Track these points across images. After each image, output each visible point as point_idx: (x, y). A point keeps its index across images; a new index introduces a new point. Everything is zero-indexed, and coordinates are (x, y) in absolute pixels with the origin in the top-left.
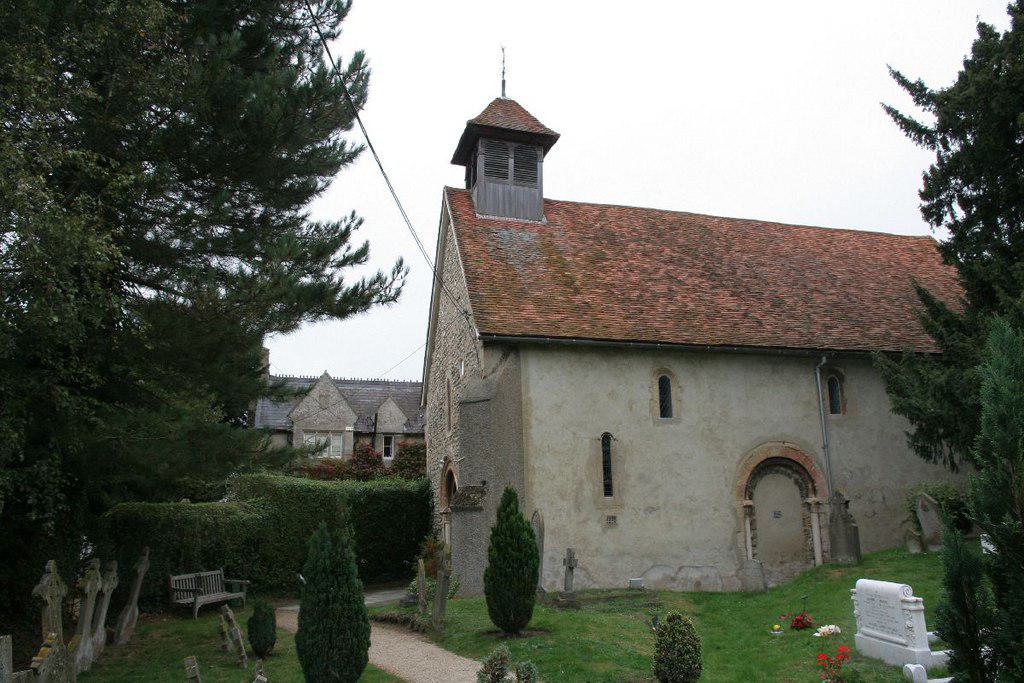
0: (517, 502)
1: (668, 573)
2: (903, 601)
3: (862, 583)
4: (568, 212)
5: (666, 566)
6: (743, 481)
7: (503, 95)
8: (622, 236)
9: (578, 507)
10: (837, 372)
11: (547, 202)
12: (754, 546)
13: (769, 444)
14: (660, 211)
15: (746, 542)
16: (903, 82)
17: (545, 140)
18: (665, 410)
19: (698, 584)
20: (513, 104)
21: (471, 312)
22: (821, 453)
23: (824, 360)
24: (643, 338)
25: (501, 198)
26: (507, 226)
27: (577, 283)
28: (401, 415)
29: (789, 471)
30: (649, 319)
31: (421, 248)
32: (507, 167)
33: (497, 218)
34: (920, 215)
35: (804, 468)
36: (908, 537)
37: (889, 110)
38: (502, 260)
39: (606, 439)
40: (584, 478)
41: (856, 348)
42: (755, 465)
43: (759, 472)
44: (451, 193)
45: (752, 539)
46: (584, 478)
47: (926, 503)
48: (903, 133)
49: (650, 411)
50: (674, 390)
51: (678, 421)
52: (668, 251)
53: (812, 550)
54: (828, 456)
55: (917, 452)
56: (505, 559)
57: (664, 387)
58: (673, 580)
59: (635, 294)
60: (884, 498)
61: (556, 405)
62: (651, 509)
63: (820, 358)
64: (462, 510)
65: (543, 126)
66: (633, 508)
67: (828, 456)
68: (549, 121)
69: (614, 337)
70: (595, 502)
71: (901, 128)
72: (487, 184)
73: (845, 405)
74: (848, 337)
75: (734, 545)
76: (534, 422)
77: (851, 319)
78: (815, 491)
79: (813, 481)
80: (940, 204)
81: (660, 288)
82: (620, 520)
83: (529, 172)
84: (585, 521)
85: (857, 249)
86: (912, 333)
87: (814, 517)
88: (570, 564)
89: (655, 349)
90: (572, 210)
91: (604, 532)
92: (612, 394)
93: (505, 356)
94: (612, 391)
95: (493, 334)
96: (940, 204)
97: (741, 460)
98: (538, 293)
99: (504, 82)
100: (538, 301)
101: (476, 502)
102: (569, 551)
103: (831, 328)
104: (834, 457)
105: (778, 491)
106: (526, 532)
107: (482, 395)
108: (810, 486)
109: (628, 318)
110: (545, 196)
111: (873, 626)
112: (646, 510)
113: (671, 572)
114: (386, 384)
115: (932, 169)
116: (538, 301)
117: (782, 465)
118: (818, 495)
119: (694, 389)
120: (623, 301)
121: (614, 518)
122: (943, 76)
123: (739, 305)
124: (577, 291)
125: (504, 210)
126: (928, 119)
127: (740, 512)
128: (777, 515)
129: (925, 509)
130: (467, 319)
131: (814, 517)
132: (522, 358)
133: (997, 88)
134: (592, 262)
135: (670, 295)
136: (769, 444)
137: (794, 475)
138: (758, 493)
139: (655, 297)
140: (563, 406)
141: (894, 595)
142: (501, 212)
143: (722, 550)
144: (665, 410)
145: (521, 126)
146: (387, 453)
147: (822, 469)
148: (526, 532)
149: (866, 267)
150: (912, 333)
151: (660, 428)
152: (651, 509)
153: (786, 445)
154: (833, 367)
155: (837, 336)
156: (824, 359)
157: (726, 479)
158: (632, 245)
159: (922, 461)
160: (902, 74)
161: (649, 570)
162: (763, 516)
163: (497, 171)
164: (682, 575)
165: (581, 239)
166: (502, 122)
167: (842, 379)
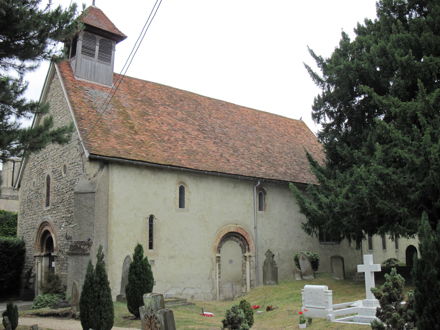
2: (326, 292)
3: (307, 286)
6: (217, 244)
7: (94, 4)
8: (156, 102)
10: (264, 191)
11: (115, 74)
12: (219, 277)
13: (231, 225)
14: (174, 89)
16: (314, 55)
18: (182, 205)
20: (99, 11)
23: (259, 183)
24: (174, 164)
25: (89, 69)
26: (93, 87)
27: (136, 128)
29: (237, 239)
32: (94, 51)
34: (311, 116)
36: (294, 272)
37: (307, 66)
38: (94, 109)
39: (151, 218)
41: (273, 178)
43: (224, 239)
45: (219, 274)
47: (304, 256)
48: (311, 79)
52: (179, 113)
53: (245, 279)
54: (256, 233)
55: (305, 230)
57: (182, 190)
58: (181, 294)
59: (166, 138)
60: (279, 254)
62: (172, 257)
64: (76, 254)
65: (117, 29)
67: (256, 233)
69: (160, 162)
71: (311, 76)
72: (82, 59)
74: (269, 172)
75: (210, 277)
77: (270, 162)
78: (249, 250)
79: (248, 245)
80: (320, 114)
81: (179, 135)
83: (107, 55)
85: (270, 123)
86: (297, 172)
87: (248, 263)
89: (180, 171)
93: (102, 168)
95: (97, 155)
96: (320, 114)
100: (117, 137)
101: (84, 250)
103: (261, 166)
104: (259, 232)
105: (232, 249)
108: (247, 247)
109: (164, 151)
110: (114, 71)
111: (309, 303)
112: (169, 258)
113: (180, 291)
115: (319, 97)
116: (117, 137)
117: (234, 236)
118: (251, 252)
119: (196, 191)
121: (153, 261)
122: (327, 54)
123: (218, 149)
124: (136, 133)
125: (91, 77)
126: (320, 73)
127: (214, 260)
128: (231, 261)
129: (303, 259)
132: (110, 172)
133: (352, 69)
134: (141, 116)
135: (184, 140)
136: (231, 225)
138: (222, 250)
139: (177, 140)
141: (322, 290)
142: (89, 77)
144: (182, 205)
145: (105, 28)
147: (253, 239)
149: (275, 134)
150: (297, 172)
152: (172, 257)
153: (238, 226)
154: (262, 186)
155: (264, 171)
158: (161, 108)
159: (307, 235)
160: (314, 51)
162: (224, 261)
165: (134, 101)
167: (265, 194)
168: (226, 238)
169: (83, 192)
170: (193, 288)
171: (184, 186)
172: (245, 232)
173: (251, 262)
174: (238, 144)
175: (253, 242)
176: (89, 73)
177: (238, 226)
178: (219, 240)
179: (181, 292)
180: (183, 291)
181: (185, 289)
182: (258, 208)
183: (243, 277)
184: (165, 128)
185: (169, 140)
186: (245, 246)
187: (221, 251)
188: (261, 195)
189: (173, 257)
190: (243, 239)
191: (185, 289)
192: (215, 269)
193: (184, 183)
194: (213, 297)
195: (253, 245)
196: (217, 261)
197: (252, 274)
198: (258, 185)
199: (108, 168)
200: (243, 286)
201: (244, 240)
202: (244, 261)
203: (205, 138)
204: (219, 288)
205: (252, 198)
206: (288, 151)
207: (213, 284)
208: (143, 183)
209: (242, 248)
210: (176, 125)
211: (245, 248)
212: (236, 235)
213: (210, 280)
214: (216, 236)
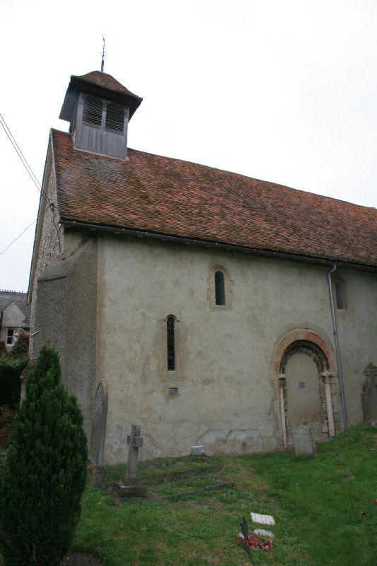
0: (57, 367)
1: (220, 436)
4: (145, 157)
5: (219, 430)
6: (278, 359)
7: (102, 70)
9: (144, 379)
12: (286, 411)
15: (280, 408)
17: (132, 102)
18: (220, 299)
19: (244, 444)
21: (56, 205)
22: (332, 338)
25: (94, 138)
26: (97, 157)
28: (22, 315)
29: (310, 352)
30: (207, 228)
31: (22, 158)
32: (100, 117)
33: (90, 152)
35: (321, 350)
39: (171, 320)
40: (150, 353)
42: (287, 346)
43: (289, 352)
44: (55, 134)
45: (285, 405)
46: (150, 353)
49: (208, 298)
50: (227, 284)
51: (231, 308)
53: (326, 412)
54: (337, 340)
56: (29, 458)
57: (219, 279)
58: (225, 442)
59: (196, 211)
61: (128, 288)
62: (207, 382)
63: (332, 267)
66: (193, 381)
67: (337, 340)
68: (133, 88)
70: (160, 375)
73: (346, 304)
76: (107, 302)
79: (327, 359)
81: (216, 210)
82: (180, 391)
84: (151, 392)
87: (327, 387)
88: (135, 441)
90: (150, 159)
91: (167, 401)
92: (176, 283)
93: (84, 242)
94: (177, 280)
97: (278, 341)
98: (118, 200)
99: (103, 62)
102: (134, 427)
104: (340, 339)
105: (302, 366)
106: (66, 416)
107: (59, 274)
110: (129, 146)
113: (222, 435)
114: (14, 294)
119: (246, 284)
120: (187, 214)
121: (176, 389)
128: (302, 385)
130: (53, 210)
131: (327, 387)
137: (313, 355)
138: (288, 367)
139: (211, 214)
140: (134, 287)
143: (263, 415)
144: (220, 299)
146: (10, 341)
148: (66, 416)
151: (215, 313)
152: (207, 382)
153: (309, 330)
156: (335, 267)
157: (266, 356)
161: (205, 434)
162: (292, 386)
163: (92, 119)
164: (231, 437)
166: (99, 82)
168: (291, 349)
169: (49, 279)
170: (244, 430)
171: (222, 271)
172: (320, 341)
173: (333, 386)
174: (299, 223)
175: (333, 355)
176: (94, 143)
177: (309, 330)
178: (282, 352)
179: (225, 438)
180: (227, 436)
181: (231, 432)
182: (336, 305)
183: (322, 408)
184: (196, 201)
185: (200, 213)
186: (322, 361)
187: (286, 369)
188: (339, 284)
189: (209, 382)
190: (318, 350)
191: (231, 432)
192: (278, 398)
193: (221, 267)
194: (278, 442)
195: (335, 359)
196: (280, 385)
197: (335, 404)
198: (333, 270)
199: (95, 242)
200: (322, 422)
201: (319, 351)
202: (322, 384)
203: (253, 215)
204: (286, 426)
205: (327, 290)
206: (366, 235)
207: (277, 421)
208: (155, 266)
209: (317, 364)
210: (211, 199)
211: (322, 365)
212: (307, 344)
213: (271, 415)
214: (276, 347)
